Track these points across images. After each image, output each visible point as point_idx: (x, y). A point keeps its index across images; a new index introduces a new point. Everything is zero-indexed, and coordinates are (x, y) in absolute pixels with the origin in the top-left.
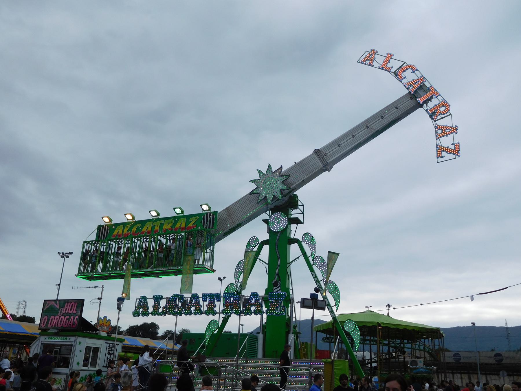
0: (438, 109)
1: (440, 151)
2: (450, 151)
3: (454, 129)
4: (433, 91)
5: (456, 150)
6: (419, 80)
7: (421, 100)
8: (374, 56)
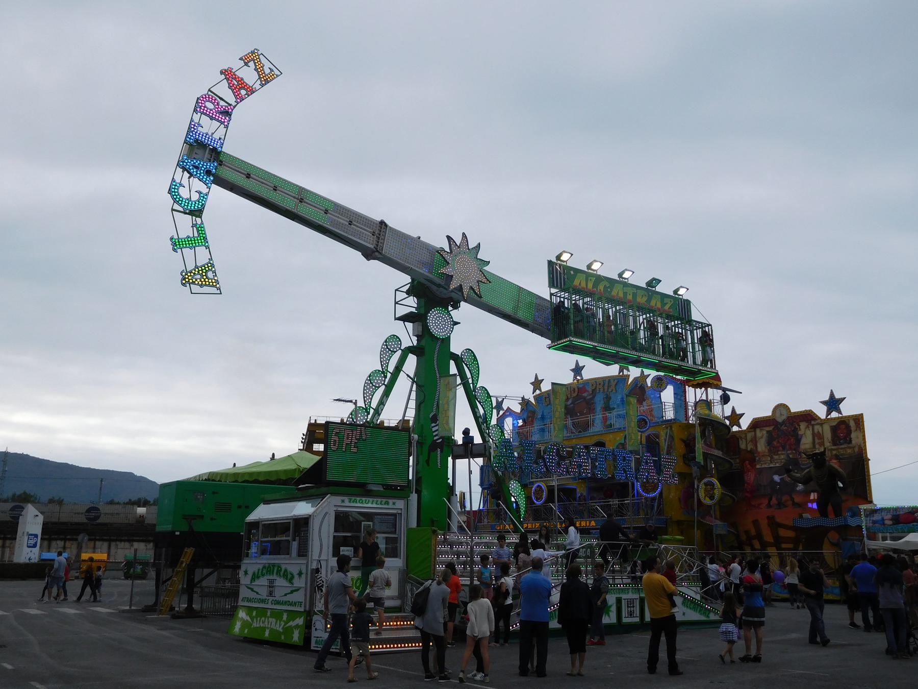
0: (214, 111)
1: (267, 77)
2: (259, 64)
3: (217, 107)
4: (193, 134)
5: (252, 57)
6: (189, 165)
7: (218, 144)
8: (193, 272)
